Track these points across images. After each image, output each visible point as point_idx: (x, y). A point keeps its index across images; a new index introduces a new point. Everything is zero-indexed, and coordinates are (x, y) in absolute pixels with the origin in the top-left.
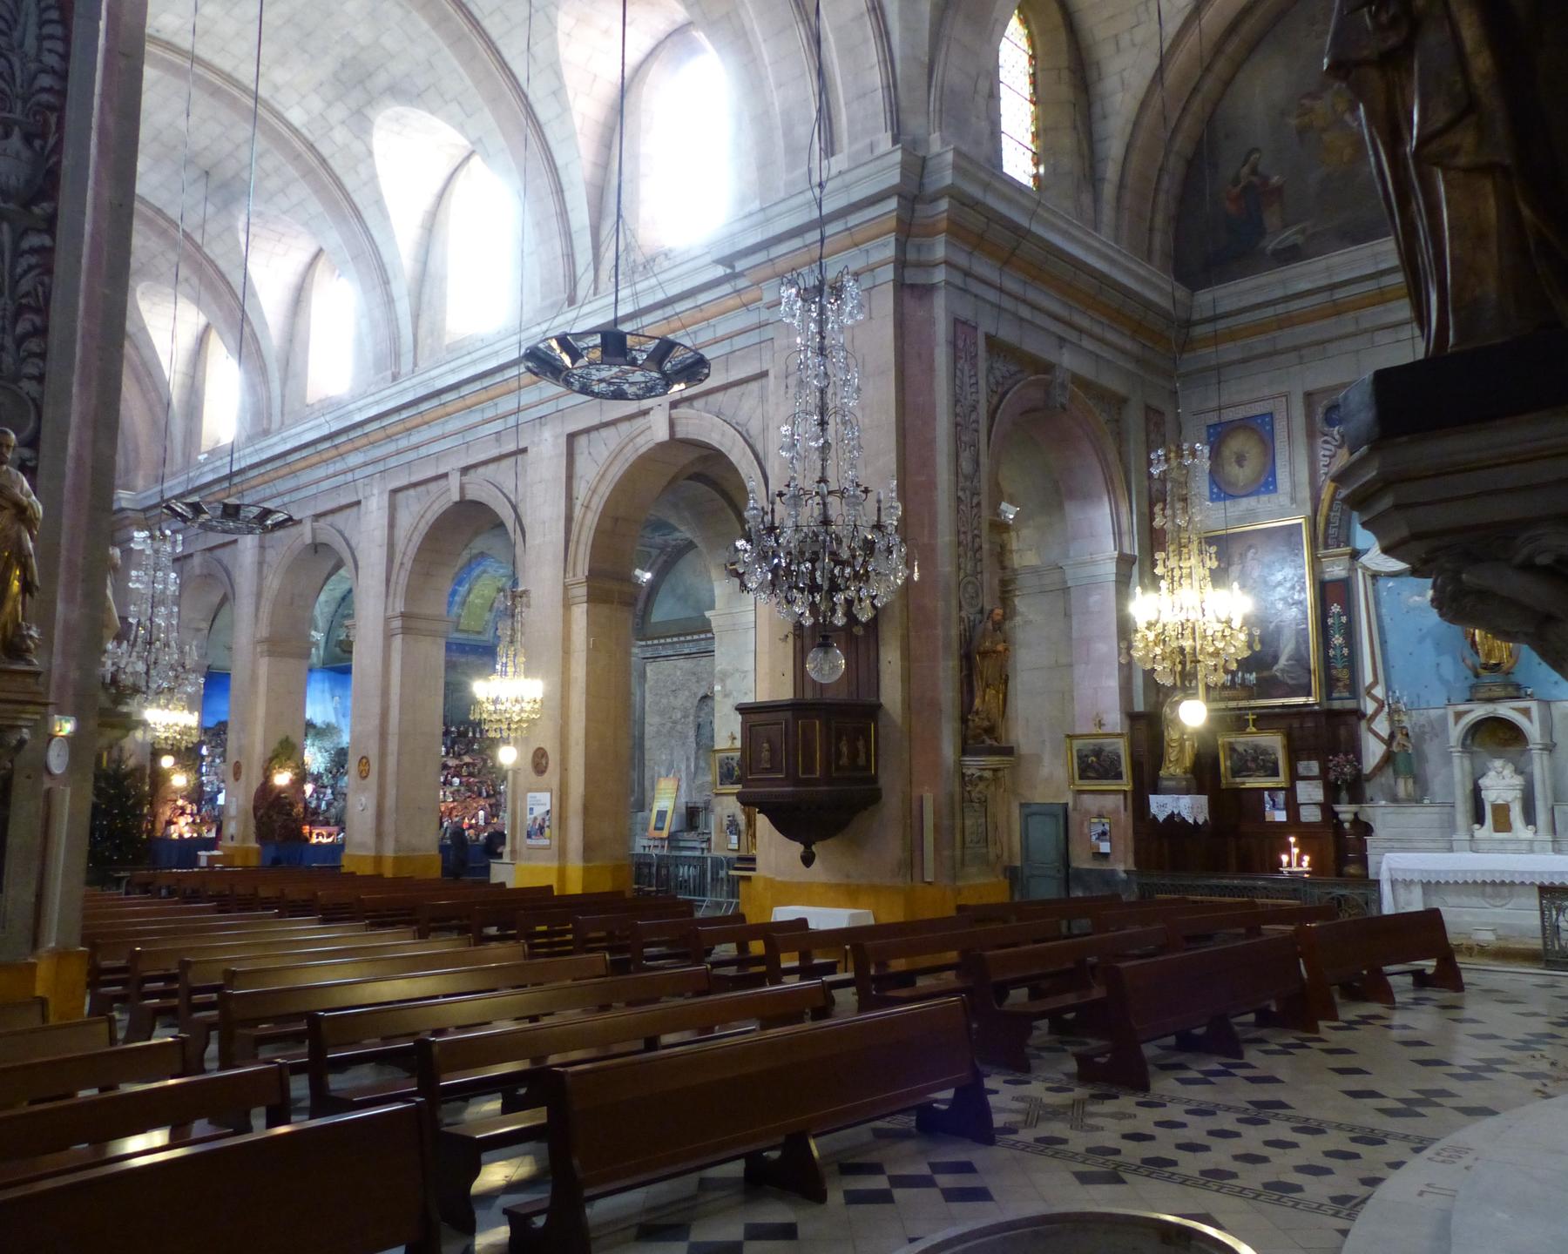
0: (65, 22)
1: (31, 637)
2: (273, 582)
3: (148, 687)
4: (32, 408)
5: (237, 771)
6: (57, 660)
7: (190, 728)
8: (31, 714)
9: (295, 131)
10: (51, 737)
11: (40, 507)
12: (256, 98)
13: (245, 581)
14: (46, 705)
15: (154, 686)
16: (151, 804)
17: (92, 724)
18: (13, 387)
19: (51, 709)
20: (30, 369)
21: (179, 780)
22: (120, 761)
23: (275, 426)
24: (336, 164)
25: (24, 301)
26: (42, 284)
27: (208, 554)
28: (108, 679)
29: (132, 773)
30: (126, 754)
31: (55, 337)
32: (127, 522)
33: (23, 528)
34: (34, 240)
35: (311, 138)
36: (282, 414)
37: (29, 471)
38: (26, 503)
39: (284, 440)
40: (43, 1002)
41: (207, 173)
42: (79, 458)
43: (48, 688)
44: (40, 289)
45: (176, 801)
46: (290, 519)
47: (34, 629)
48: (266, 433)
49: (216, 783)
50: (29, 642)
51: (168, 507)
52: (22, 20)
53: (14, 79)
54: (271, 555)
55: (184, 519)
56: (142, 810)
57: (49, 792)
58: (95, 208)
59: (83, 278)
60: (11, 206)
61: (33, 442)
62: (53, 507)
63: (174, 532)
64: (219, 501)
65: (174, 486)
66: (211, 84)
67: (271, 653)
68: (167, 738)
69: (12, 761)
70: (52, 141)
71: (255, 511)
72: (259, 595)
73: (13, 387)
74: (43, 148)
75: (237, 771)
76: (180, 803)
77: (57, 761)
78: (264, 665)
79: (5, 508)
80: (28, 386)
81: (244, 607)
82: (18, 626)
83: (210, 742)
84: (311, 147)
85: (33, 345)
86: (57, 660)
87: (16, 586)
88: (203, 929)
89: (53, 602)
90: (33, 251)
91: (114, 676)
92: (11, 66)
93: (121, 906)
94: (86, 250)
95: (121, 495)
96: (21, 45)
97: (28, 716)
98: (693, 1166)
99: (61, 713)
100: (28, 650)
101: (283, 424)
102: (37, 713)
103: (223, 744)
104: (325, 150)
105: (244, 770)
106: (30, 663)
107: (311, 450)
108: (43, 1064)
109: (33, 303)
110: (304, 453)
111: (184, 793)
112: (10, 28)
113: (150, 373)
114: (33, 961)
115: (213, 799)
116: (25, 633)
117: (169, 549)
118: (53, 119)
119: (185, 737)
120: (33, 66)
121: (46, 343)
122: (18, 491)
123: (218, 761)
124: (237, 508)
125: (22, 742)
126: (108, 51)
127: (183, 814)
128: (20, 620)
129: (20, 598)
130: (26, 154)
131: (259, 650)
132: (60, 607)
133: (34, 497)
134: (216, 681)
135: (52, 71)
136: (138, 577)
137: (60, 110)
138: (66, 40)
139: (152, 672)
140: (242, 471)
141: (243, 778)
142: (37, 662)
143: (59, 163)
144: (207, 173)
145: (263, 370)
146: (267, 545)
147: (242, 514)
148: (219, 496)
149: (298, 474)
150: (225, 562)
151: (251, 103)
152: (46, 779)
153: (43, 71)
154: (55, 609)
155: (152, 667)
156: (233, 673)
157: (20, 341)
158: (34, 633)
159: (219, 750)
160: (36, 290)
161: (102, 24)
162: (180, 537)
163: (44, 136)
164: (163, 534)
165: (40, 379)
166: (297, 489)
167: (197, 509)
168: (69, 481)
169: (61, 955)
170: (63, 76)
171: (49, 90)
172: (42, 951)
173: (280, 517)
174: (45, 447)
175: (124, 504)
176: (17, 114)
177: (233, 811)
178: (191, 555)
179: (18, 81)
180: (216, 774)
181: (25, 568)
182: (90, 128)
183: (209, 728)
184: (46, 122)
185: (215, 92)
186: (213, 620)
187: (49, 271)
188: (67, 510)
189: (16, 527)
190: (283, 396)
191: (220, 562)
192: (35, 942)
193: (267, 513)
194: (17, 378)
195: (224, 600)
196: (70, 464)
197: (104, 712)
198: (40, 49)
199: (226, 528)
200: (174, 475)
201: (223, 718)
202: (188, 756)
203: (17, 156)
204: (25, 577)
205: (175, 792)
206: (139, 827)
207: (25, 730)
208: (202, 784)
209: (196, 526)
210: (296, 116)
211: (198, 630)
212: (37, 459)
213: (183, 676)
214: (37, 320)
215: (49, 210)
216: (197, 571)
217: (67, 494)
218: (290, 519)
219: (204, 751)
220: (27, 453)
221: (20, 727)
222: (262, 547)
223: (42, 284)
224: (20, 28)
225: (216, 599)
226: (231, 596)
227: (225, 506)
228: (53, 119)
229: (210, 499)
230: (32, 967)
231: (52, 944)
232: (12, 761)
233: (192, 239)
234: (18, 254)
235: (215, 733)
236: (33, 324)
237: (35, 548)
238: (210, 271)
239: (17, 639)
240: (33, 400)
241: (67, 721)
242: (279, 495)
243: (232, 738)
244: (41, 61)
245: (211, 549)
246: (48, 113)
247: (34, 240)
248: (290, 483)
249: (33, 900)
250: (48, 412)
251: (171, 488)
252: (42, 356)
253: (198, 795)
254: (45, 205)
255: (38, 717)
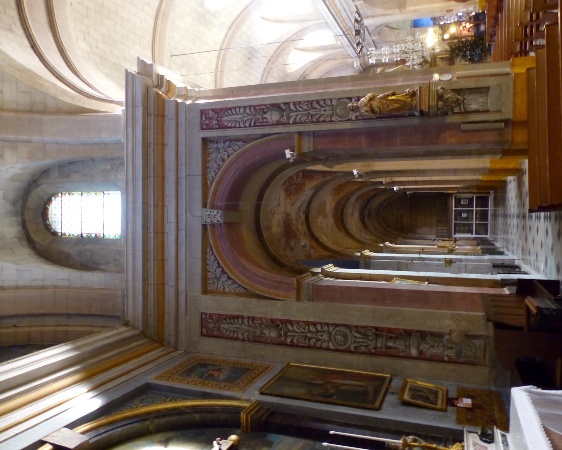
0: (230, 109)
1: (409, 91)
2: (379, 11)
3: (421, 50)
4: (340, 101)
5: (449, 11)
6: (415, 82)
7: (434, 31)
8: (433, 88)
9: (227, 34)
10: (440, 80)
11: (369, 94)
12: (221, 50)
13: (380, 21)
14: (430, 84)
15: (420, 49)
16: (462, 38)
17: (435, 69)
18: (335, 106)
19: (431, 82)
20: (329, 103)
21: (453, 30)
22: (446, 51)
23: (323, 21)
24: (232, 19)
25: (310, 107)
26: (304, 103)
27: (372, 35)
28: (420, 66)
29: (451, 47)
30: (444, 49)
31: (318, 98)
32: (364, 62)
33: (376, 98)
34: (292, 107)
35: (227, 29)
36: (319, 19)
37: (358, 99)
38: (369, 98)
39: (328, 17)
40: (528, 70)
41: (248, 59)
42: (352, 86)
43: (425, 84)
44: (305, 104)
45: (461, 30)
46: (357, 12)
47: (406, 90)
48: (327, 23)
49: (454, 17)
50: (410, 91)
51: (359, 53)
52: (234, 119)
53: (251, 119)
54: (369, 13)
55: (362, 47)
56: (464, 41)
57: (458, 78)
58: (278, 93)
59: (299, 93)
60: (285, 114)
61: (350, 99)
62: (369, 91)
63: (368, 51)
64: (355, 38)
65: (350, 51)
66: (222, 63)
67: (405, 7)
68: (438, 38)
69: (448, 90)
70: (264, 107)
71: (356, 24)
72: (384, 15)
73: (335, 106)
74: (266, 109)
75: (449, 11)
76: (461, 28)
77: (447, 77)
78: (410, 8)
79: (371, 103)
80: (334, 102)
81: (388, 19)
82: (406, 95)
83: (438, 22)
84: (230, 28)
85: (322, 103)
86: (415, 82)
87: (393, 97)
88: (509, 16)
89: (397, 86)
90: (295, 107)
91: (419, 64)
92: (247, 120)
93: (498, 45)
94: (291, 94)
95: (356, 66)
96: (241, 118)
97: (434, 88)
98: (409, 310)
99: (432, 78)
100: (413, 91)
101: (322, 19)
102: (432, 86)
103: (439, 18)
104: (229, 24)
105: (449, 8)
106: (417, 90)
107: (330, 7)
108: (548, 67)
109: (310, 105)
110: (331, 9)
111: (458, 27)
112: (237, 122)
113: (316, 64)
114: (513, 74)
115: (460, 17)
116: (408, 93)
117: (374, 51)
118: (257, 108)
119: (437, 32)
120: (245, 115)
121: (321, 100)
122: (365, 101)
123: (445, 18)
124: (356, 31)
125: (442, 88)
126: (233, 96)
127: (465, 27)
128: (404, 95)
129: (397, 96)
130: (269, 113)
131: (404, 11)
132: (398, 84)
133: (366, 97)
134: (416, 24)
135: (245, 110)
136: (384, 60)
137: (254, 107)
138: (235, 108)
139: (416, 50)
140: (343, 31)
141: (452, 8)
142: (417, 88)
143: (269, 104)
144: (248, 59)
145: (306, 28)
146: (366, 16)
147: (357, 29)
148: (353, 38)
149: (339, 10)
150: (373, 29)
151: (223, 51)
152: (453, 80)
153: (245, 112)
154: (399, 86)
155: (414, 50)
156: (413, 18)
157: (322, 106)
158: (408, 90)
159: (442, 18)
160: (306, 105)
161: (227, 99)
162: (370, 49)
163: (263, 109)
164: (369, 55)
165: (331, 100)
166: (344, 9)
167: (358, 44)
168: (359, 88)
169: (513, 65)
170: (245, 107)
171: (250, 110)
172: (511, 72)
173: (357, 16)
174: (350, 96)
175: (359, 64)
176: (260, 116)
177: (465, 10)
178: (373, 41)
179: (251, 118)
180: (450, 17)
181: (388, 96)
182: (256, 98)
183: (434, 23)
184: (259, 109)
185: (224, 61)
186: (394, 29)
187: (300, 102)
188: (368, 87)
189: (376, 100)
190: (313, 20)
191: (374, 31)
192: (508, 74)
193: (356, 21)
194: (332, 105)
195: (387, 26)
196: (354, 88)
197: (431, 66)
198: (240, 114)
199: (363, 33)
200: (346, 51)
201: (429, 18)
202: (444, 28)
203: (271, 115)
204: (391, 95)
205: (457, 31)
206: (470, 41)
207: (438, 88)
208: (454, 22)
209: (364, 43)
210: (222, 35)
211: (398, 33)
212: (354, 97)
213: (416, 40)
214: (314, 103)
215: (283, 105)
216: (378, 37)
217: (363, 87)
218: (357, 12)
219: (442, 23)
220: (353, 100)
221: (437, 89)
222: (367, 17)
223: (304, 103)
224: (237, 119)
225: (387, 29)
226: (386, 25)
227: (356, 35)
228: (257, 108)
229: (354, 40)
230: (515, 74)
231: (509, 69)
232: (448, 90)
233: (270, 59)
234: (297, 111)
235: (435, 21)
236: (316, 104)
237: (382, 94)
238: (278, 51)
239: (410, 94)
240: (337, 101)
241: (434, 76)
242: (349, 17)
243: (436, 15)
244: (243, 113)
245: (370, 34)
246: (256, 109)
247: (292, 107)
248: (343, 12)
249: (493, 77)
250: (341, 96)
251: (353, 54)
252: (324, 100)
253: (459, 23)
254: (282, 106)
255: (434, 85)
